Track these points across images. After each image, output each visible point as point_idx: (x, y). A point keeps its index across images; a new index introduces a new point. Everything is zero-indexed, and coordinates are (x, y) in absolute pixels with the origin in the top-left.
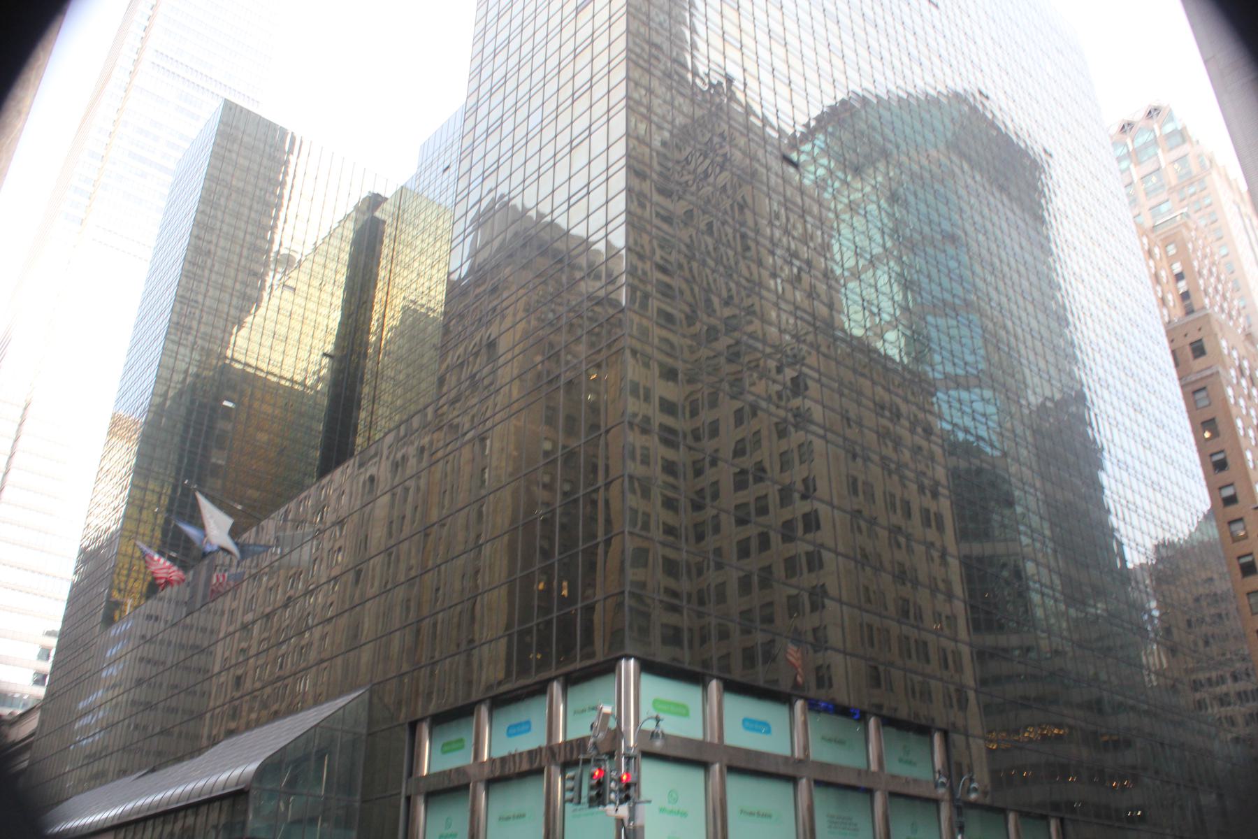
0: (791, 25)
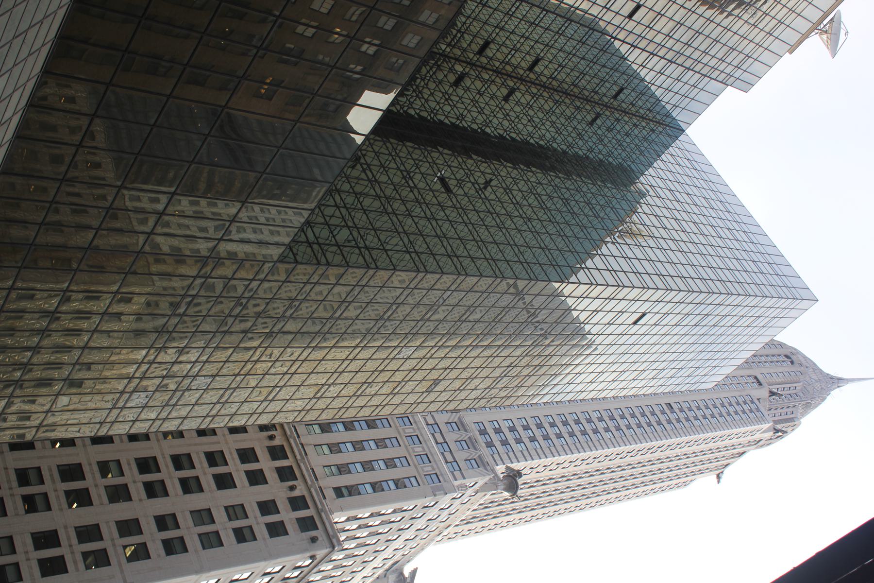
0: (622, 305)
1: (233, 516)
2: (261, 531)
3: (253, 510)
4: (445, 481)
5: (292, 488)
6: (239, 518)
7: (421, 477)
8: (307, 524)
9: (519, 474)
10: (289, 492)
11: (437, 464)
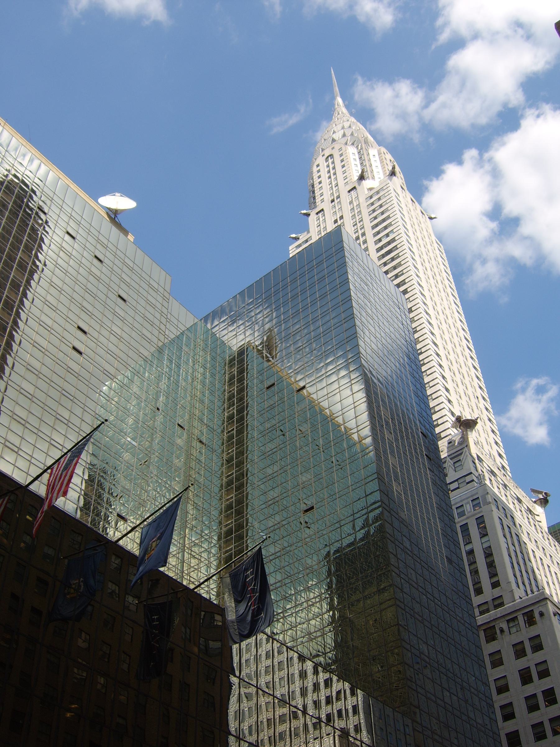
1: (349, 298)
2: (539, 657)
3: (522, 663)
4: (477, 493)
5: (502, 631)
6: (349, 295)
7: (476, 514)
8: (530, 620)
9: (458, 419)
10: (505, 633)
11: (464, 500)
